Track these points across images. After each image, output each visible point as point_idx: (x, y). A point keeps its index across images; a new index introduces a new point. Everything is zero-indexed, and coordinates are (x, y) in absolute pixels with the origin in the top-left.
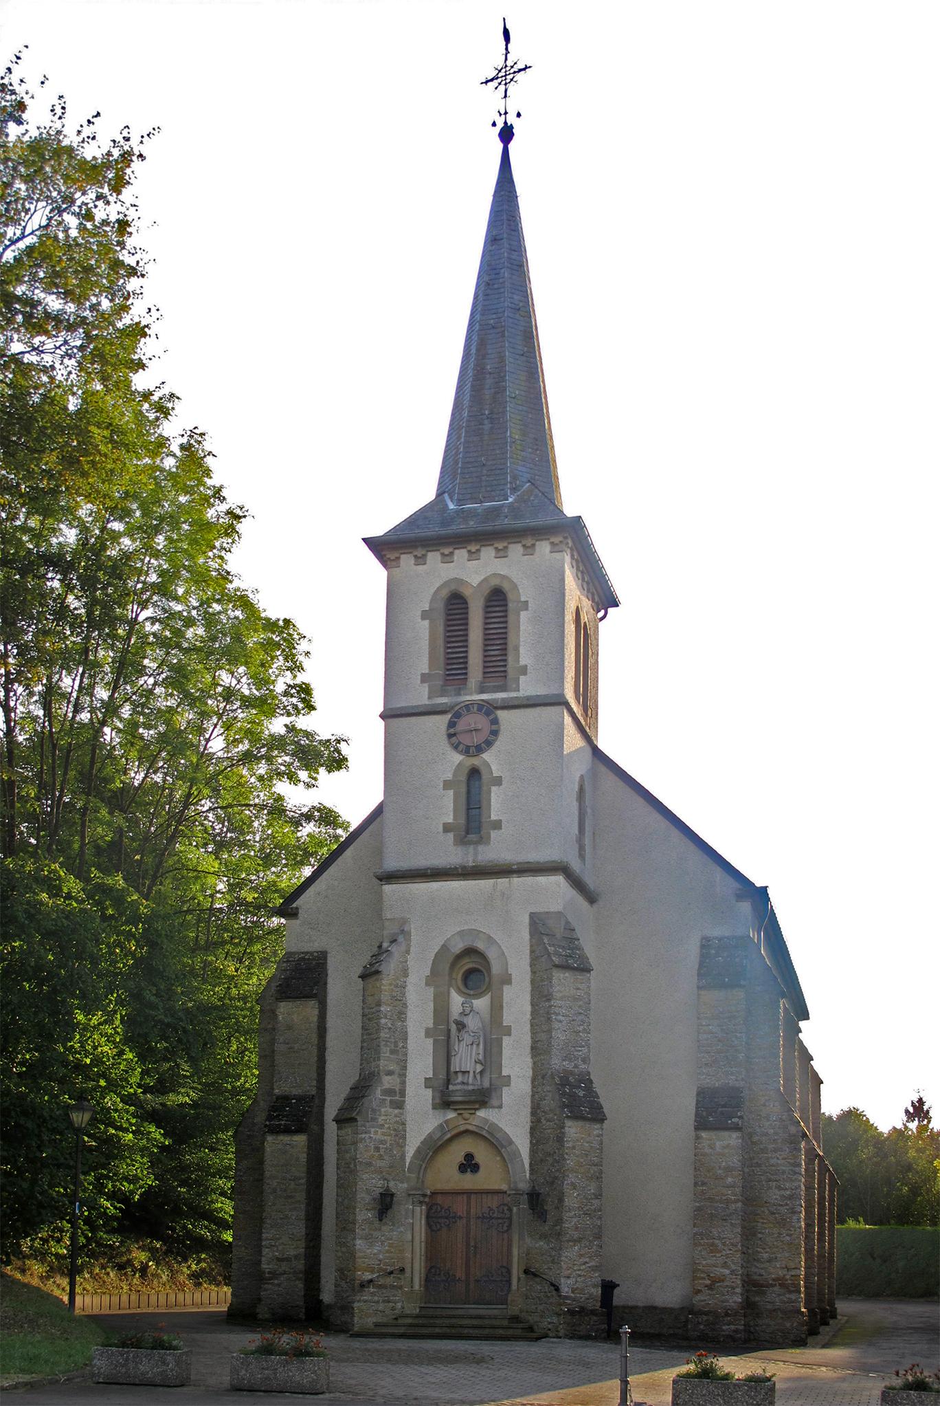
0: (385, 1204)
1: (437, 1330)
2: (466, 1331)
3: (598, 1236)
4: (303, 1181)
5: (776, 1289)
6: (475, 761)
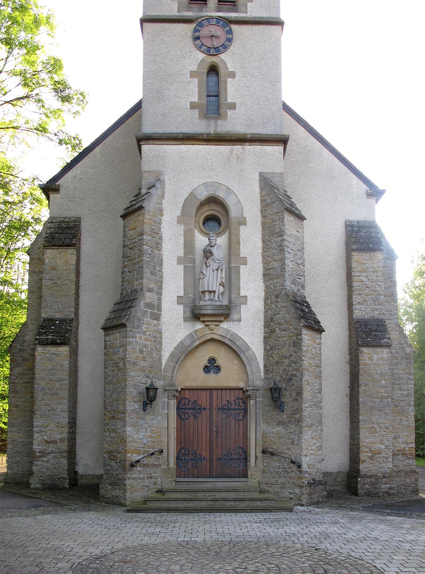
0: (149, 396)
1: (204, 504)
2: (228, 504)
3: (320, 423)
4: (66, 382)
5: (400, 457)
6: (215, 59)
